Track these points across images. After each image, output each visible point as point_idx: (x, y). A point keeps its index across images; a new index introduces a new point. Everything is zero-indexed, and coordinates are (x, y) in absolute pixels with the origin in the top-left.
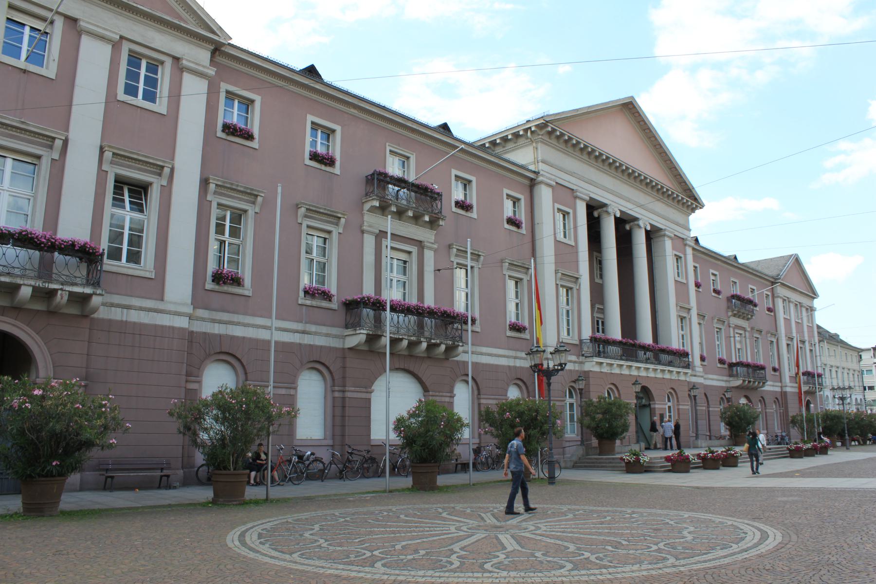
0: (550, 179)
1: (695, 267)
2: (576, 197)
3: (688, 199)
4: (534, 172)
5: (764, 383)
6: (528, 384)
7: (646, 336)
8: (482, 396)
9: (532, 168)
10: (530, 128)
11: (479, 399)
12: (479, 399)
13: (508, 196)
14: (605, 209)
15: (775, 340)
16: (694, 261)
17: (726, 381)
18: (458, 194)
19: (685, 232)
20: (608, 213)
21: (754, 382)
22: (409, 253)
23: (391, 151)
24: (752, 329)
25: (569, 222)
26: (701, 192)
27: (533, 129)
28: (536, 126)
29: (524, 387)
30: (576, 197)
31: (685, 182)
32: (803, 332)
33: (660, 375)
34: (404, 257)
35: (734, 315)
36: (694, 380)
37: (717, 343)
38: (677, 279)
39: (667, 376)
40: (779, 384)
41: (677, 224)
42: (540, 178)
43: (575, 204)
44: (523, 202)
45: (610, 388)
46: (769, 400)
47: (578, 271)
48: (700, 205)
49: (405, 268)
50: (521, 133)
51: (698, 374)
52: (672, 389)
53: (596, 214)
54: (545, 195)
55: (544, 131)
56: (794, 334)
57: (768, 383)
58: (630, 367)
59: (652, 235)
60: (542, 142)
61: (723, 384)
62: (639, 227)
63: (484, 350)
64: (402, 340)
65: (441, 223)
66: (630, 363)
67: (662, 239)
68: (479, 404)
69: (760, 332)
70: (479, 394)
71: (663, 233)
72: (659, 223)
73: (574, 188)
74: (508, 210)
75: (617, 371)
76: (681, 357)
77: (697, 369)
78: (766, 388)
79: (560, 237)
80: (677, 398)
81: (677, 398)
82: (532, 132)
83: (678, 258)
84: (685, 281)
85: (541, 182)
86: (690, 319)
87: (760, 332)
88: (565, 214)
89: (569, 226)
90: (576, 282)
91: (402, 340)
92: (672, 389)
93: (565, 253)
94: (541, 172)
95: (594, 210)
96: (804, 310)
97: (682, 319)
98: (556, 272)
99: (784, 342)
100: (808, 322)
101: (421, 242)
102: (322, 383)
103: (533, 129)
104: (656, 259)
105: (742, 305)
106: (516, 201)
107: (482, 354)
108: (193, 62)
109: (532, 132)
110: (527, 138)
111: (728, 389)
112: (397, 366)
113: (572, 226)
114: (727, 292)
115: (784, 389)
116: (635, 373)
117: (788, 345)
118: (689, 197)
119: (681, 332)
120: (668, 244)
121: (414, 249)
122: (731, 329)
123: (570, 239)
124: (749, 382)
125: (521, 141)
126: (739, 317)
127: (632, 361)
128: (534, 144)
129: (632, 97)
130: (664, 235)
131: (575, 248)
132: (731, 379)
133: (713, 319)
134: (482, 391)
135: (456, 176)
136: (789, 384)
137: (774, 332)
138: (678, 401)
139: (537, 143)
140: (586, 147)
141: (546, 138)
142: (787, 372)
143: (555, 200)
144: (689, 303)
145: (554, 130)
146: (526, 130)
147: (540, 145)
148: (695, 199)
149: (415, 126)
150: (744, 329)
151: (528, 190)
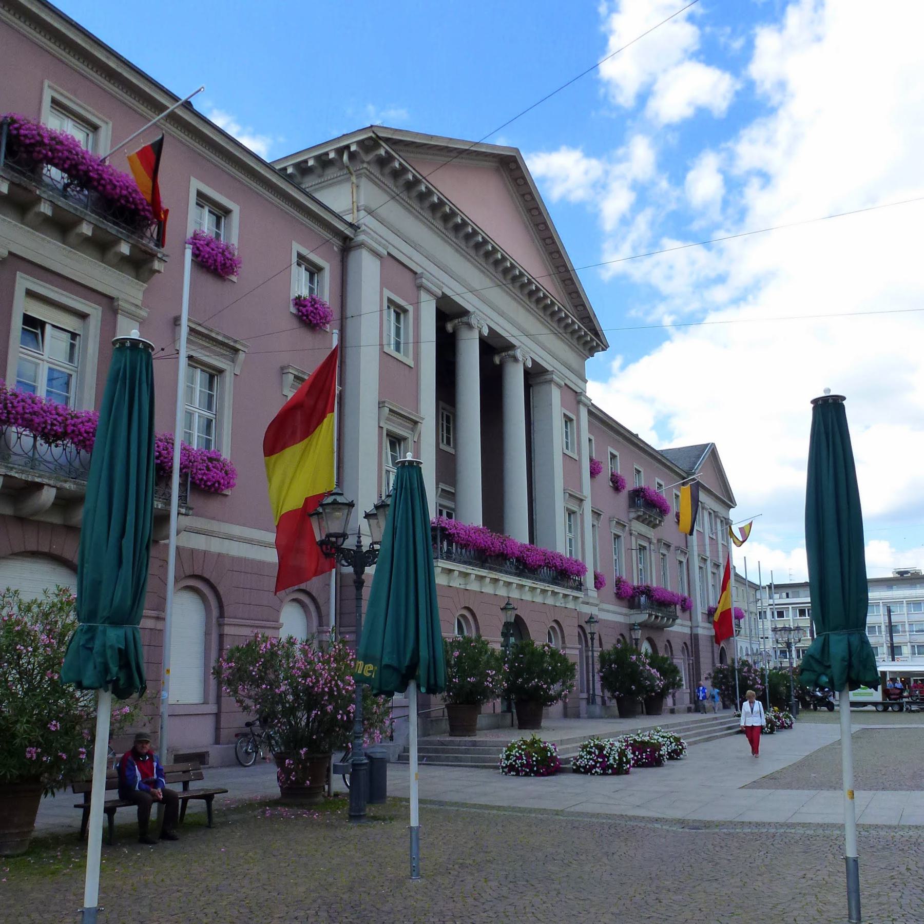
0: (379, 244)
1: (590, 440)
2: (420, 287)
3: (587, 337)
4: (351, 225)
5: (674, 620)
6: (321, 601)
7: (518, 531)
8: (227, 620)
9: (349, 218)
10: (347, 147)
11: (220, 625)
12: (220, 625)
13: (301, 258)
14: (465, 319)
15: (685, 561)
16: (590, 431)
17: (626, 615)
18: (201, 222)
19: (580, 382)
20: (470, 326)
21: (662, 618)
22: (83, 316)
23: (54, 101)
24: (659, 541)
25: (406, 328)
26: (604, 322)
27: (353, 148)
28: (360, 143)
29: (312, 608)
30: (420, 287)
31: (584, 305)
32: (717, 551)
33: (539, 599)
34: (70, 323)
35: (638, 518)
36: (587, 610)
37: (615, 557)
38: (566, 452)
39: (550, 601)
40: (689, 623)
41: (569, 368)
42: (362, 237)
43: (418, 297)
44: (327, 274)
45: (463, 616)
46: (677, 646)
47: (417, 410)
48: (605, 347)
49: (72, 346)
50: (332, 155)
51: (591, 601)
52: (556, 621)
53: (449, 327)
54: (368, 271)
55: (370, 157)
56: (708, 554)
57: (678, 621)
58: (496, 581)
59: (535, 376)
60: (367, 177)
61: (620, 619)
62: (516, 359)
63: (237, 530)
64: (40, 486)
65: (157, 265)
66: (494, 575)
67: (545, 387)
68: (221, 636)
69: (668, 546)
70: (222, 615)
71: (548, 377)
72: (547, 362)
73: (419, 270)
74: (300, 286)
75: (474, 586)
76: (564, 573)
77: (590, 593)
78: (675, 628)
79: (391, 349)
80: (563, 637)
81: (563, 637)
82: (352, 156)
83: (568, 420)
84: (576, 457)
85: (361, 245)
86: (582, 515)
87: (668, 546)
88: (400, 312)
89: (406, 333)
90: (413, 430)
91: (40, 486)
92: (556, 621)
93: (395, 370)
94: (363, 227)
95: (449, 316)
96: (719, 522)
97: (571, 513)
98: (381, 405)
99: (696, 562)
100: (723, 539)
101: (111, 299)
102: (203, 613)
103: (353, 148)
104: (536, 416)
105: (648, 505)
106: (314, 271)
107: (231, 538)
108: (287, 493)
109: (352, 156)
110: (343, 167)
111: (632, 627)
112: (32, 547)
113: (411, 340)
114: (631, 484)
115: (695, 631)
116: (502, 592)
117: (700, 568)
118: (590, 330)
119: (568, 534)
120: (556, 395)
121: (95, 311)
122: (633, 538)
123: (406, 354)
124: (657, 617)
125: (331, 173)
126: (643, 522)
127: (501, 572)
128: (354, 179)
129: (517, 150)
130: (551, 381)
131: (414, 371)
132: (632, 612)
133: (610, 520)
134: (228, 610)
135: (200, 194)
136: (701, 624)
137: (683, 546)
138: (564, 642)
139: (359, 176)
140: (441, 203)
141: (375, 170)
142: (700, 610)
143: (384, 283)
144: (581, 491)
145: (389, 158)
146: (340, 151)
147: (364, 182)
148: (597, 333)
149: (112, 64)
150: (649, 541)
151: (338, 259)
